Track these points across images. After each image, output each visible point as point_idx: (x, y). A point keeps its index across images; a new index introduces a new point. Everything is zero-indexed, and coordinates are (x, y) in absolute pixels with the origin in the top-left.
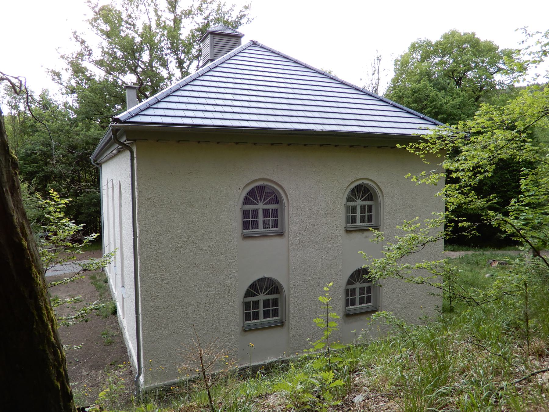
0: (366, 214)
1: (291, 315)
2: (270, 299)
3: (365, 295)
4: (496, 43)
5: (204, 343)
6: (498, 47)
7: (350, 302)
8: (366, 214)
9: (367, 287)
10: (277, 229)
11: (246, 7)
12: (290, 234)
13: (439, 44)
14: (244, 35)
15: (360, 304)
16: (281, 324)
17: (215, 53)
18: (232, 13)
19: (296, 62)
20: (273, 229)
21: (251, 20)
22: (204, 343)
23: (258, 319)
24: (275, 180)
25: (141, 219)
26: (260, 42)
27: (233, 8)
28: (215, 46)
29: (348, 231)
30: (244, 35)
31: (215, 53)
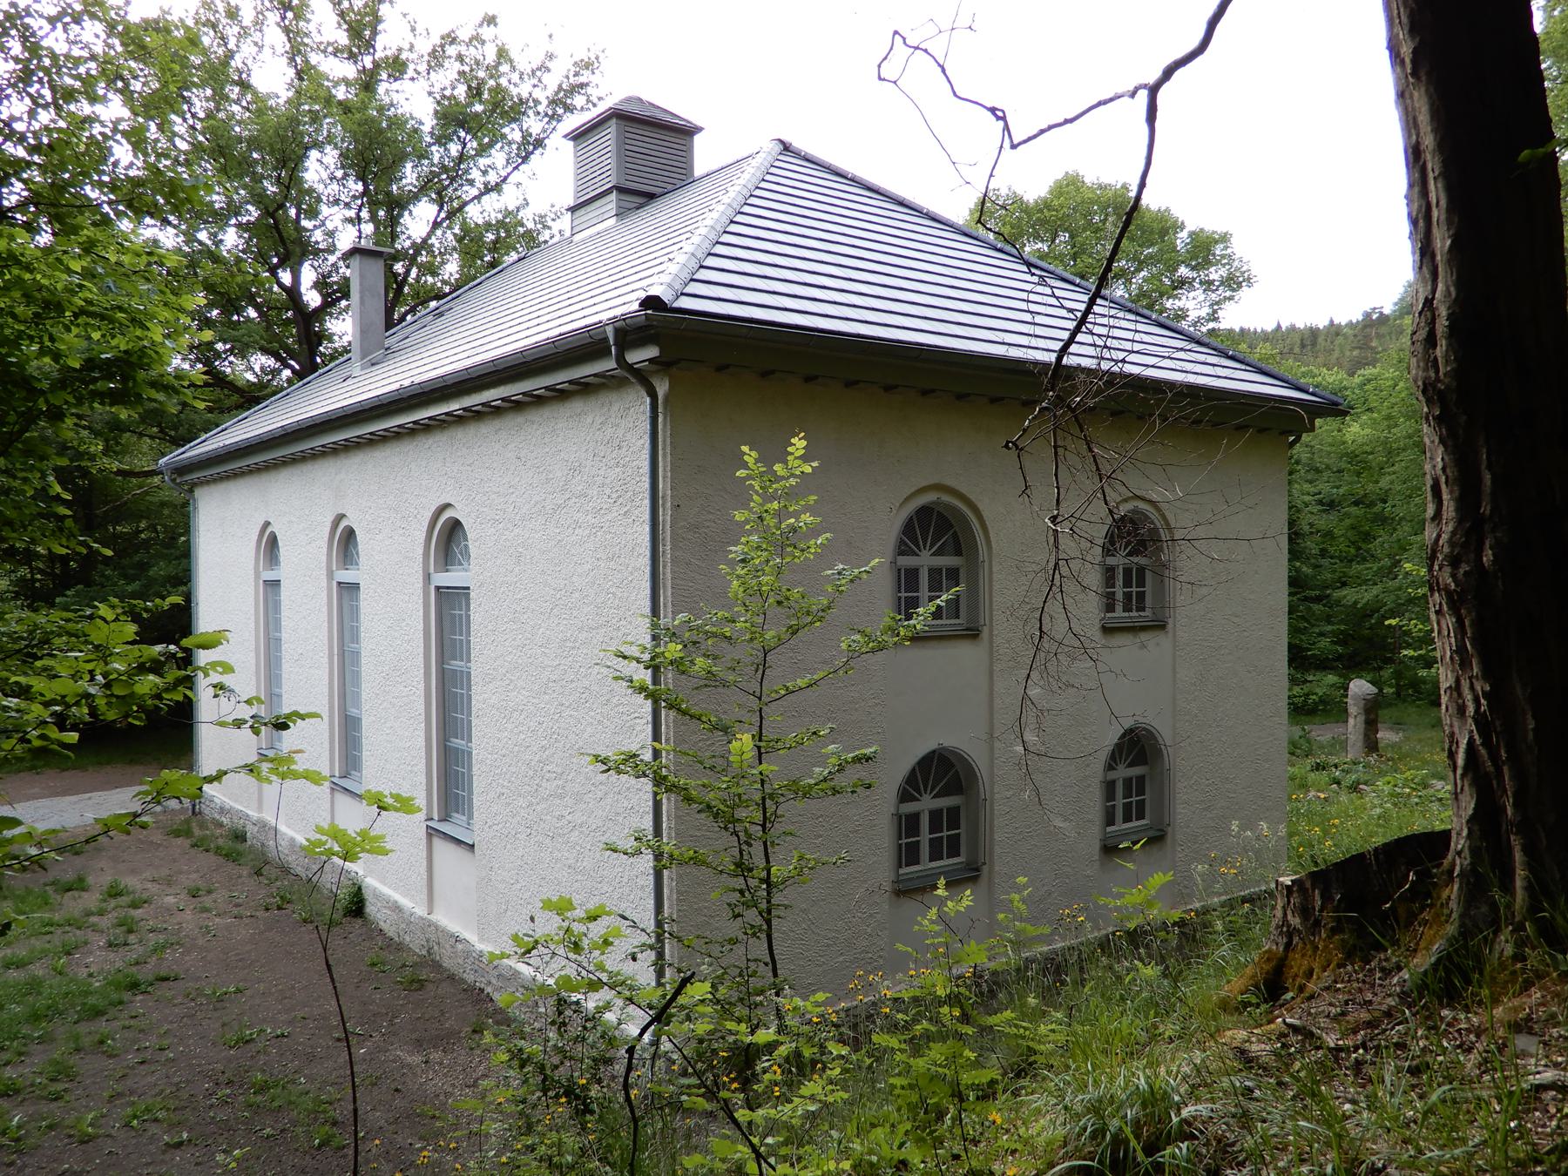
0: (1134, 589)
1: (997, 850)
2: (942, 810)
3: (945, 833)
4: (1179, 213)
5: (812, 927)
6: (1183, 223)
7: (909, 854)
8: (1134, 589)
9: (949, 809)
10: (957, 621)
11: (588, 65)
12: (995, 632)
13: (1045, 205)
14: (700, 129)
15: (931, 860)
16: (1157, 838)
17: (628, 171)
18: (546, 78)
19: (901, 203)
20: (948, 622)
21: (595, 101)
22: (812, 927)
23: (918, 863)
24: (964, 491)
25: (679, 582)
26: (797, 143)
27: (548, 64)
28: (628, 153)
29: (1107, 630)
30: (700, 129)
31: (628, 171)
